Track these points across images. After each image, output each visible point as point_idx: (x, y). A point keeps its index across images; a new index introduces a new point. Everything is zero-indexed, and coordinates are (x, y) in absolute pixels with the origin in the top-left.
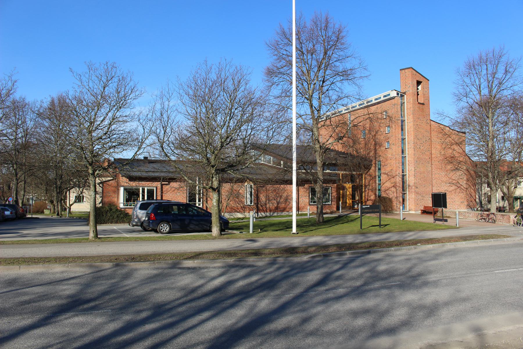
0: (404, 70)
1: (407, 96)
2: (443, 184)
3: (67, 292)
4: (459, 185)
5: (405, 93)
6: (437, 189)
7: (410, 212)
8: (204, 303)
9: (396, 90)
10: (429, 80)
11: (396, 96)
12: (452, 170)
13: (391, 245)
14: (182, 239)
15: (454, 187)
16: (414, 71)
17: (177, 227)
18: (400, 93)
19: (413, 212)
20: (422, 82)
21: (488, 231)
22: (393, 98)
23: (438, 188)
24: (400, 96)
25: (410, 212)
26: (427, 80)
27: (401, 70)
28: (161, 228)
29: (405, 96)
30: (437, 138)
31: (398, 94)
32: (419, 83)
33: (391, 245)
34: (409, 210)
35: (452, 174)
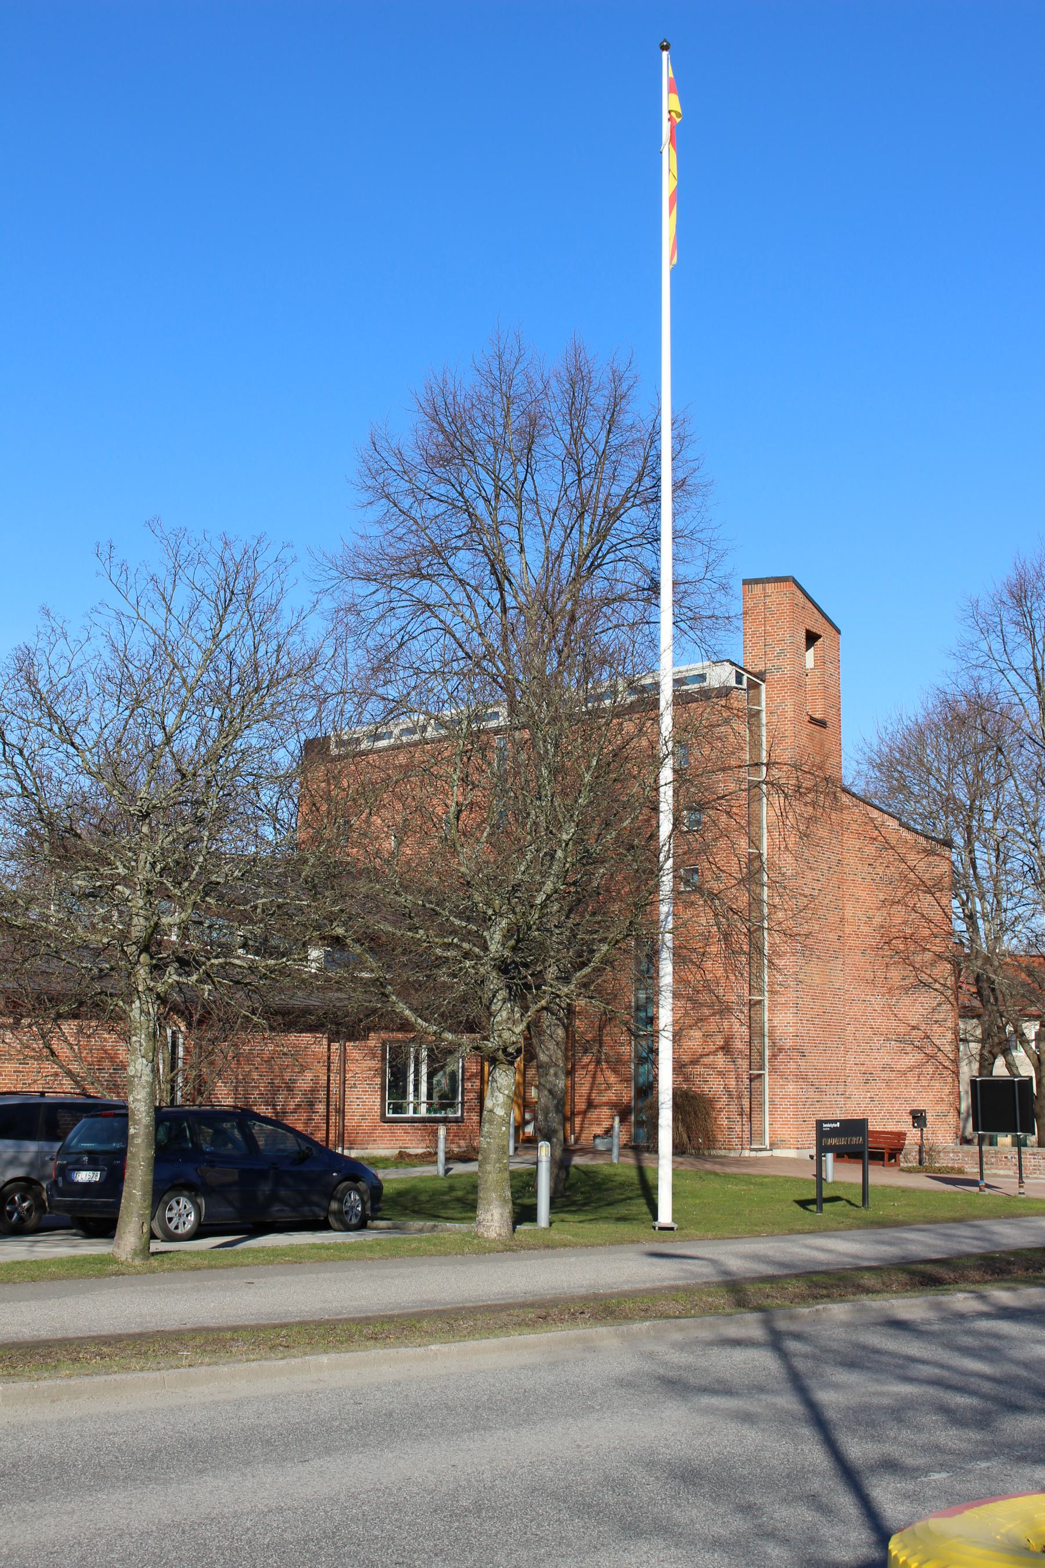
0: (760, 586)
1: (770, 687)
2: (878, 1041)
3: (961, 1296)
4: (929, 1050)
5: (761, 676)
6: (857, 1061)
7: (777, 1153)
8: (979, 1365)
9: (732, 664)
10: (839, 632)
11: (734, 684)
12: (906, 990)
13: (970, 1238)
14: (296, 1258)
15: (913, 1058)
16: (799, 593)
17: (226, 1211)
18: (746, 676)
19: (791, 1153)
20: (820, 637)
21: (817, 1249)
22: (724, 692)
23: (863, 1058)
24: (745, 686)
25: (777, 1153)
26: (834, 632)
27: (746, 582)
28: (168, 1214)
29: (763, 686)
30: (861, 859)
31: (739, 679)
32: (812, 638)
33: (970, 1238)
34: (773, 1146)
35: (906, 1000)
